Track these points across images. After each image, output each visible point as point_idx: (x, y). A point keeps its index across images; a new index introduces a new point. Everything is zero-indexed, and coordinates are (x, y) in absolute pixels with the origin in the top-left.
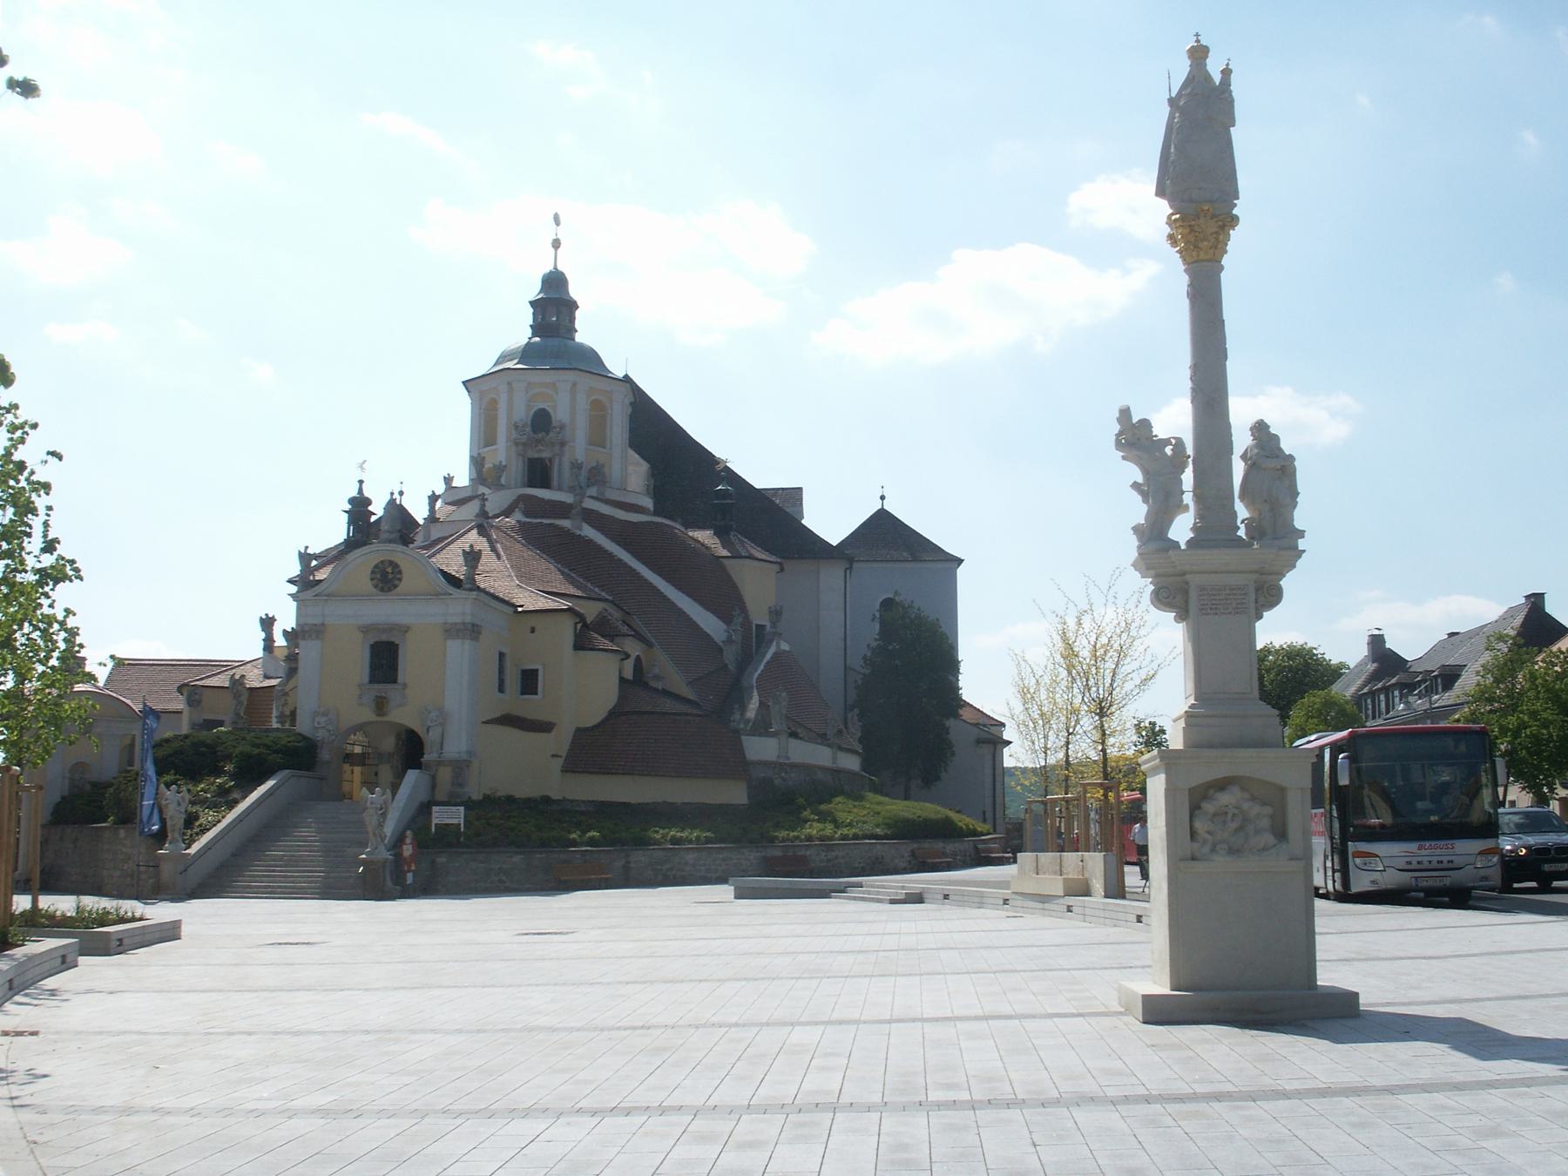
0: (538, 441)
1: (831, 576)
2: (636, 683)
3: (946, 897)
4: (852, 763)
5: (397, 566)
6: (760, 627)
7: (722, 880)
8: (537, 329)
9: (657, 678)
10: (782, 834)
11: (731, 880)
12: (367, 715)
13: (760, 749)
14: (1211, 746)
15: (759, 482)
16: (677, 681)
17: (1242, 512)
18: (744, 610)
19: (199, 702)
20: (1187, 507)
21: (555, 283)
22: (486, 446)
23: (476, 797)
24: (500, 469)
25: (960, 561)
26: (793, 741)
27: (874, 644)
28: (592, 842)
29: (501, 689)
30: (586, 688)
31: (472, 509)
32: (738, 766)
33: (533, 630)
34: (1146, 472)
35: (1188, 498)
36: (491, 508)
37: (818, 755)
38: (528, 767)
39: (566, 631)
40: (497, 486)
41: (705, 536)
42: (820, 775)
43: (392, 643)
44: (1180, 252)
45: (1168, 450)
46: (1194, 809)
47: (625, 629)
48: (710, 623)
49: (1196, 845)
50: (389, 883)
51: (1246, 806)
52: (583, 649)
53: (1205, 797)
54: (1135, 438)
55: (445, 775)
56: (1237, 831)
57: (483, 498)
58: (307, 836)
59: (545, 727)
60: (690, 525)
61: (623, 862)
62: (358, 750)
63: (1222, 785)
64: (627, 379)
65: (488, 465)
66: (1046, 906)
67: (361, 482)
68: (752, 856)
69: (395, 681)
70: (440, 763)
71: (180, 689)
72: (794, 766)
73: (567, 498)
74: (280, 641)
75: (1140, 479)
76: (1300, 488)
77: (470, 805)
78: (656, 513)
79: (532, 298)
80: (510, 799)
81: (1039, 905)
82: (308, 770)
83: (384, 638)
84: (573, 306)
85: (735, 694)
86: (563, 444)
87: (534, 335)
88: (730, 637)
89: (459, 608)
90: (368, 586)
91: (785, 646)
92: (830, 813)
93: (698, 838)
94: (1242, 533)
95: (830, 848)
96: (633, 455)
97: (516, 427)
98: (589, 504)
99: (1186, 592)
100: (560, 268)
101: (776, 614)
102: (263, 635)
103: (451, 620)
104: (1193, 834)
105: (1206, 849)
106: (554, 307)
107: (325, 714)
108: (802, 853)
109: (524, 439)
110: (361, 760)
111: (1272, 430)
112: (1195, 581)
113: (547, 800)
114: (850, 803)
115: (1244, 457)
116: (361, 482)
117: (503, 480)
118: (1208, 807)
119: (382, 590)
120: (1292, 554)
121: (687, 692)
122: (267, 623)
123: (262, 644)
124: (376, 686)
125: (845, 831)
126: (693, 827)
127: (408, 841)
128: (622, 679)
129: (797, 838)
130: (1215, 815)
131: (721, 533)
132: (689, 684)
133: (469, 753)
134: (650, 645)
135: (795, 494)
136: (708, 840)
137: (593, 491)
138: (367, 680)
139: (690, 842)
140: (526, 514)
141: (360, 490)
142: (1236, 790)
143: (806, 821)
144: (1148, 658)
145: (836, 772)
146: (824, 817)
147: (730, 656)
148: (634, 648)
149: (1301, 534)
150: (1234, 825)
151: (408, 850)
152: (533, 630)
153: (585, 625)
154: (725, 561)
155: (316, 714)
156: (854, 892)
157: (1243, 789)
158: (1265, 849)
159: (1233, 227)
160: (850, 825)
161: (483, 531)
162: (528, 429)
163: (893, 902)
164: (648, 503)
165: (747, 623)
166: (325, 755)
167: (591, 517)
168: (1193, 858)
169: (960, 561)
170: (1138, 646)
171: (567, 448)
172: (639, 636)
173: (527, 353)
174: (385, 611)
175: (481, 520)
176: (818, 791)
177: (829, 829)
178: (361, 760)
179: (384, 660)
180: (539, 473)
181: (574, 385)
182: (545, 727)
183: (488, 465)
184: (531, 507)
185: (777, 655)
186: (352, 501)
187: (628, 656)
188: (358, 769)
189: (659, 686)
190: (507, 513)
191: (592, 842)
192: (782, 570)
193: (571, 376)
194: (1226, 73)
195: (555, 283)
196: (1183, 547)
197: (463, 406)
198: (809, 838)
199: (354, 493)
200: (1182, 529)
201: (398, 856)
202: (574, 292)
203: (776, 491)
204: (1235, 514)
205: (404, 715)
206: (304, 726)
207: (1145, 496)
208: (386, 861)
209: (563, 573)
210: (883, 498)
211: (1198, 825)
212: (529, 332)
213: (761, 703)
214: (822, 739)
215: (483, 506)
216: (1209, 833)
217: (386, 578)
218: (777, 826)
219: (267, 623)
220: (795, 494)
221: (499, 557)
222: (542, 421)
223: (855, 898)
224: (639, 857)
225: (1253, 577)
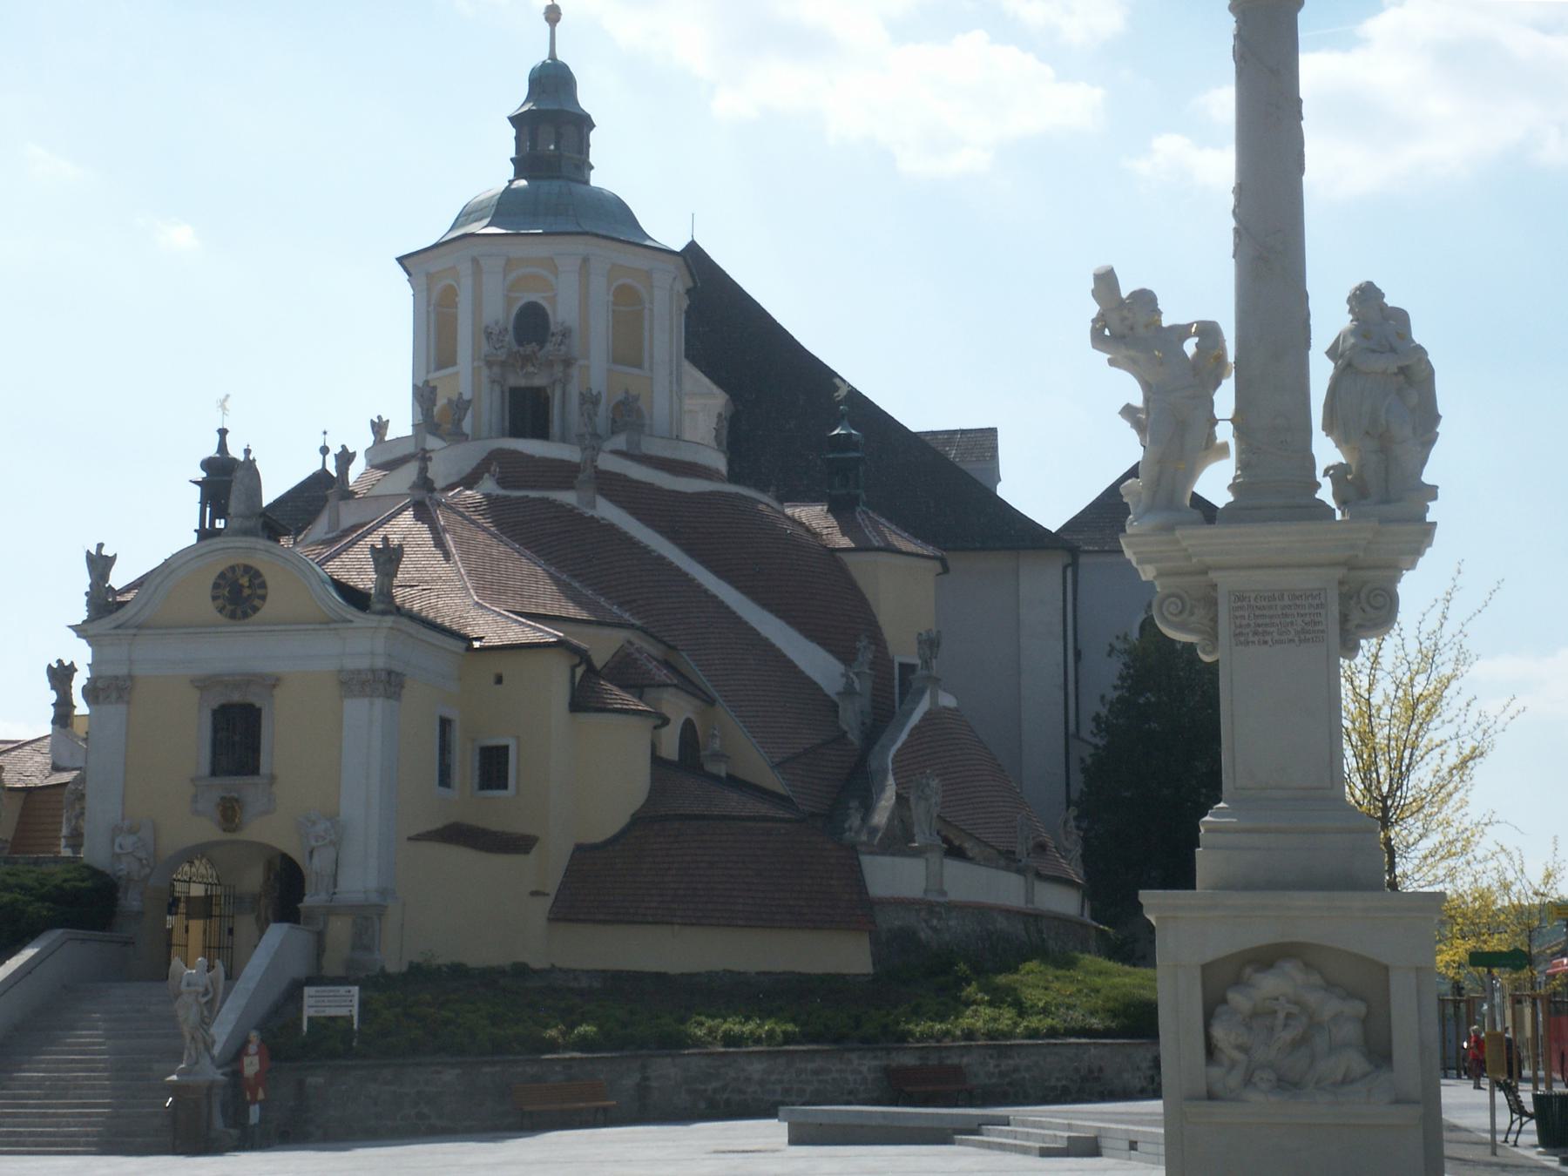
2: (683, 766)
3: (1133, 1146)
4: (1063, 902)
5: (258, 574)
6: (907, 669)
7: (768, 1112)
8: (523, 165)
9: (718, 756)
10: (919, 1028)
11: (783, 1109)
12: (207, 830)
13: (893, 877)
14: (1249, 886)
15: (914, 427)
16: (756, 765)
17: (1326, 452)
18: (877, 638)
20: (1223, 450)
21: (552, 84)
22: (440, 367)
23: (393, 967)
24: (460, 407)
26: (953, 867)
27: (1113, 695)
28: (584, 1044)
29: (445, 779)
30: (594, 775)
31: (406, 477)
32: (854, 908)
33: (499, 680)
34: (1147, 386)
35: (1225, 433)
36: (440, 472)
37: (1003, 889)
38: (491, 915)
39: (557, 680)
40: (456, 435)
41: (813, 515)
42: (1002, 923)
43: (251, 706)
45: (1190, 347)
47: (662, 675)
48: (816, 663)
49: (1216, 1072)
50: (218, 1123)
51: (1313, 999)
52: (586, 709)
53: (1238, 982)
54: (1126, 324)
55: (339, 930)
56: (1297, 1044)
57: (423, 457)
58: (90, 1043)
59: (518, 844)
60: (783, 499)
61: (637, 1077)
62: (197, 890)
63: (1266, 958)
64: (694, 256)
65: (441, 401)
68: (866, 1065)
69: (254, 770)
70: (331, 911)
72: (952, 907)
74: (81, 707)
75: (1137, 398)
76: (1443, 404)
77: (375, 984)
78: (733, 477)
80: (458, 970)
82: (103, 929)
83: (236, 697)
85: (857, 784)
86: (568, 363)
87: (518, 175)
88: (850, 684)
89: (366, 644)
90: (206, 608)
91: (947, 700)
92: (1011, 990)
93: (771, 1034)
94: (1326, 493)
95: (1003, 1052)
96: (695, 378)
97: (489, 335)
98: (608, 463)
99: (1211, 603)
100: (561, 56)
101: (930, 644)
102: (53, 696)
103: (351, 664)
104: (1211, 1050)
105: (1234, 1080)
106: (552, 125)
108: (954, 1060)
109: (502, 355)
110: (203, 908)
111: (1391, 301)
112: (1226, 582)
113: (521, 970)
114: (1051, 972)
115: (1332, 353)
116: (223, 433)
117: (467, 425)
118: (1239, 999)
119: (233, 616)
120: (1416, 535)
121: (773, 781)
122: (60, 676)
123: (51, 713)
124: (218, 781)
125: (1034, 1022)
126: (766, 1014)
127: (253, 1048)
128: (657, 761)
129: (947, 1033)
130: (1255, 1014)
131: (841, 509)
132: (777, 766)
133: (383, 892)
134: (711, 702)
135: (983, 442)
136: (788, 1038)
137: (620, 442)
138: (206, 768)
139: (758, 1041)
140: (502, 482)
141: (222, 446)
142: (1290, 968)
143: (967, 1004)
144: (1473, 717)
145: (1034, 918)
146: (998, 998)
147: (851, 719)
148: (678, 708)
150: (1287, 1036)
151: (251, 1065)
153: (591, 669)
154: (846, 557)
155: (116, 830)
156: (993, 1135)
157: (1308, 966)
158: (1347, 1080)
160: (1045, 1011)
161: (423, 513)
162: (509, 338)
163: (1046, 1153)
164: (719, 462)
165: (882, 659)
166: (131, 901)
167: (612, 487)
168: (1211, 1096)
170: (1453, 701)
172: (688, 686)
173: (505, 207)
175: (419, 495)
176: (998, 949)
177: (1006, 1017)
178: (203, 908)
179: (237, 734)
180: (529, 412)
181: (586, 260)
182: (518, 844)
183: (441, 401)
184: (510, 469)
185: (929, 717)
186: (207, 464)
187: (666, 721)
188: (196, 926)
190: (469, 481)
191: (584, 1044)
193: (579, 246)
195: (552, 84)
197: (397, 303)
198: (969, 1035)
199: (211, 451)
201: (236, 1075)
202: (586, 100)
204: (1310, 460)
205: (270, 828)
206: (96, 852)
207: (1139, 426)
208: (211, 1086)
209: (557, 581)
211: (1218, 1032)
212: (509, 171)
213: (898, 796)
214: (1008, 860)
215: (423, 470)
216: (1240, 1048)
218: (917, 1013)
220: (983, 442)
221: (447, 556)
222: (532, 324)
223: (1002, 1147)
224: (666, 1070)
225: (1339, 573)
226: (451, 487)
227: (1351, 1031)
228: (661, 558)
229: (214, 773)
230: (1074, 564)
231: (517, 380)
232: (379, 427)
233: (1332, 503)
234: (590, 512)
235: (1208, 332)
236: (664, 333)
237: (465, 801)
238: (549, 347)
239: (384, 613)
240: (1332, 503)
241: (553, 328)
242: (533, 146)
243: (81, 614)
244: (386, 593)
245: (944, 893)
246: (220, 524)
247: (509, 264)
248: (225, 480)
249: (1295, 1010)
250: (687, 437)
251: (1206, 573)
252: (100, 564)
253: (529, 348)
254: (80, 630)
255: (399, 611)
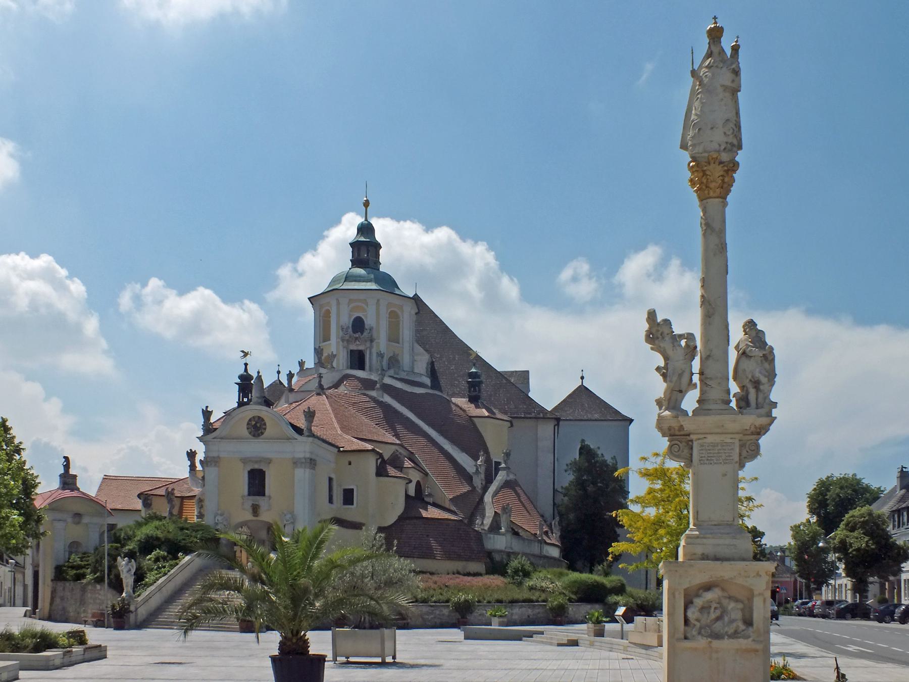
0: (356, 339)
1: (546, 430)
4: (555, 553)
11: (462, 627)
12: (248, 516)
17: (734, 388)
18: (487, 452)
19: (151, 505)
20: (695, 385)
25: (631, 421)
29: (331, 501)
33: (350, 463)
35: (696, 379)
39: (371, 464)
44: (696, 191)
46: (688, 604)
53: (698, 595)
54: (658, 333)
56: (718, 619)
63: (708, 587)
65: (325, 354)
66: (649, 652)
67: (246, 365)
69: (264, 495)
71: (139, 496)
73: (374, 377)
74: (199, 467)
78: (432, 388)
79: (351, 241)
81: (644, 651)
83: (256, 466)
84: (378, 246)
86: (372, 341)
88: (477, 469)
90: (244, 432)
96: (419, 349)
98: (388, 381)
102: (189, 463)
104: (686, 621)
107: (221, 515)
109: (347, 337)
115: (737, 348)
116: (246, 365)
118: (699, 602)
119: (254, 436)
122: (191, 455)
124: (251, 497)
128: (407, 496)
137: (391, 372)
141: (246, 370)
149: (775, 405)
152: (350, 463)
159: (735, 171)
162: (350, 330)
164: (428, 381)
165: (488, 460)
167: (388, 389)
169: (631, 421)
171: (374, 344)
174: (256, 448)
179: (257, 481)
180: (358, 360)
181: (378, 300)
186: (241, 377)
189: (431, 500)
192: (512, 425)
194: (735, 49)
196: (690, 414)
199: (242, 371)
200: (690, 402)
203: (513, 373)
205: (266, 516)
210: (582, 378)
211: (689, 614)
215: (320, 381)
217: (257, 427)
219: (191, 455)
220: (525, 375)
225: (738, 436)
226: (330, 388)
227: (738, 615)
228: (408, 418)
229: (249, 494)
230: (558, 425)
231: (353, 347)
232: (301, 364)
233: (735, 408)
234: (381, 399)
235: (690, 337)
236: (407, 332)
237: (338, 508)
238: (365, 334)
239: (308, 436)
240: (735, 408)
241: (366, 327)
242: (359, 255)
243: (201, 433)
244: (310, 430)
245: (511, 548)
246: (246, 400)
247: (350, 301)
248: (246, 384)
249: (718, 606)
250: (416, 371)
251: (689, 435)
252: (207, 414)
253: (357, 335)
254: (200, 439)
255: (313, 436)
